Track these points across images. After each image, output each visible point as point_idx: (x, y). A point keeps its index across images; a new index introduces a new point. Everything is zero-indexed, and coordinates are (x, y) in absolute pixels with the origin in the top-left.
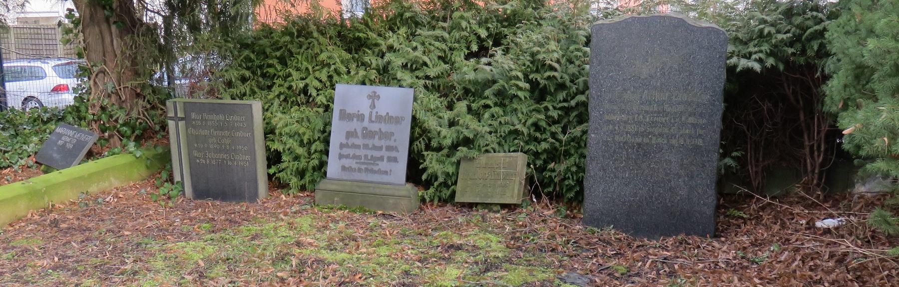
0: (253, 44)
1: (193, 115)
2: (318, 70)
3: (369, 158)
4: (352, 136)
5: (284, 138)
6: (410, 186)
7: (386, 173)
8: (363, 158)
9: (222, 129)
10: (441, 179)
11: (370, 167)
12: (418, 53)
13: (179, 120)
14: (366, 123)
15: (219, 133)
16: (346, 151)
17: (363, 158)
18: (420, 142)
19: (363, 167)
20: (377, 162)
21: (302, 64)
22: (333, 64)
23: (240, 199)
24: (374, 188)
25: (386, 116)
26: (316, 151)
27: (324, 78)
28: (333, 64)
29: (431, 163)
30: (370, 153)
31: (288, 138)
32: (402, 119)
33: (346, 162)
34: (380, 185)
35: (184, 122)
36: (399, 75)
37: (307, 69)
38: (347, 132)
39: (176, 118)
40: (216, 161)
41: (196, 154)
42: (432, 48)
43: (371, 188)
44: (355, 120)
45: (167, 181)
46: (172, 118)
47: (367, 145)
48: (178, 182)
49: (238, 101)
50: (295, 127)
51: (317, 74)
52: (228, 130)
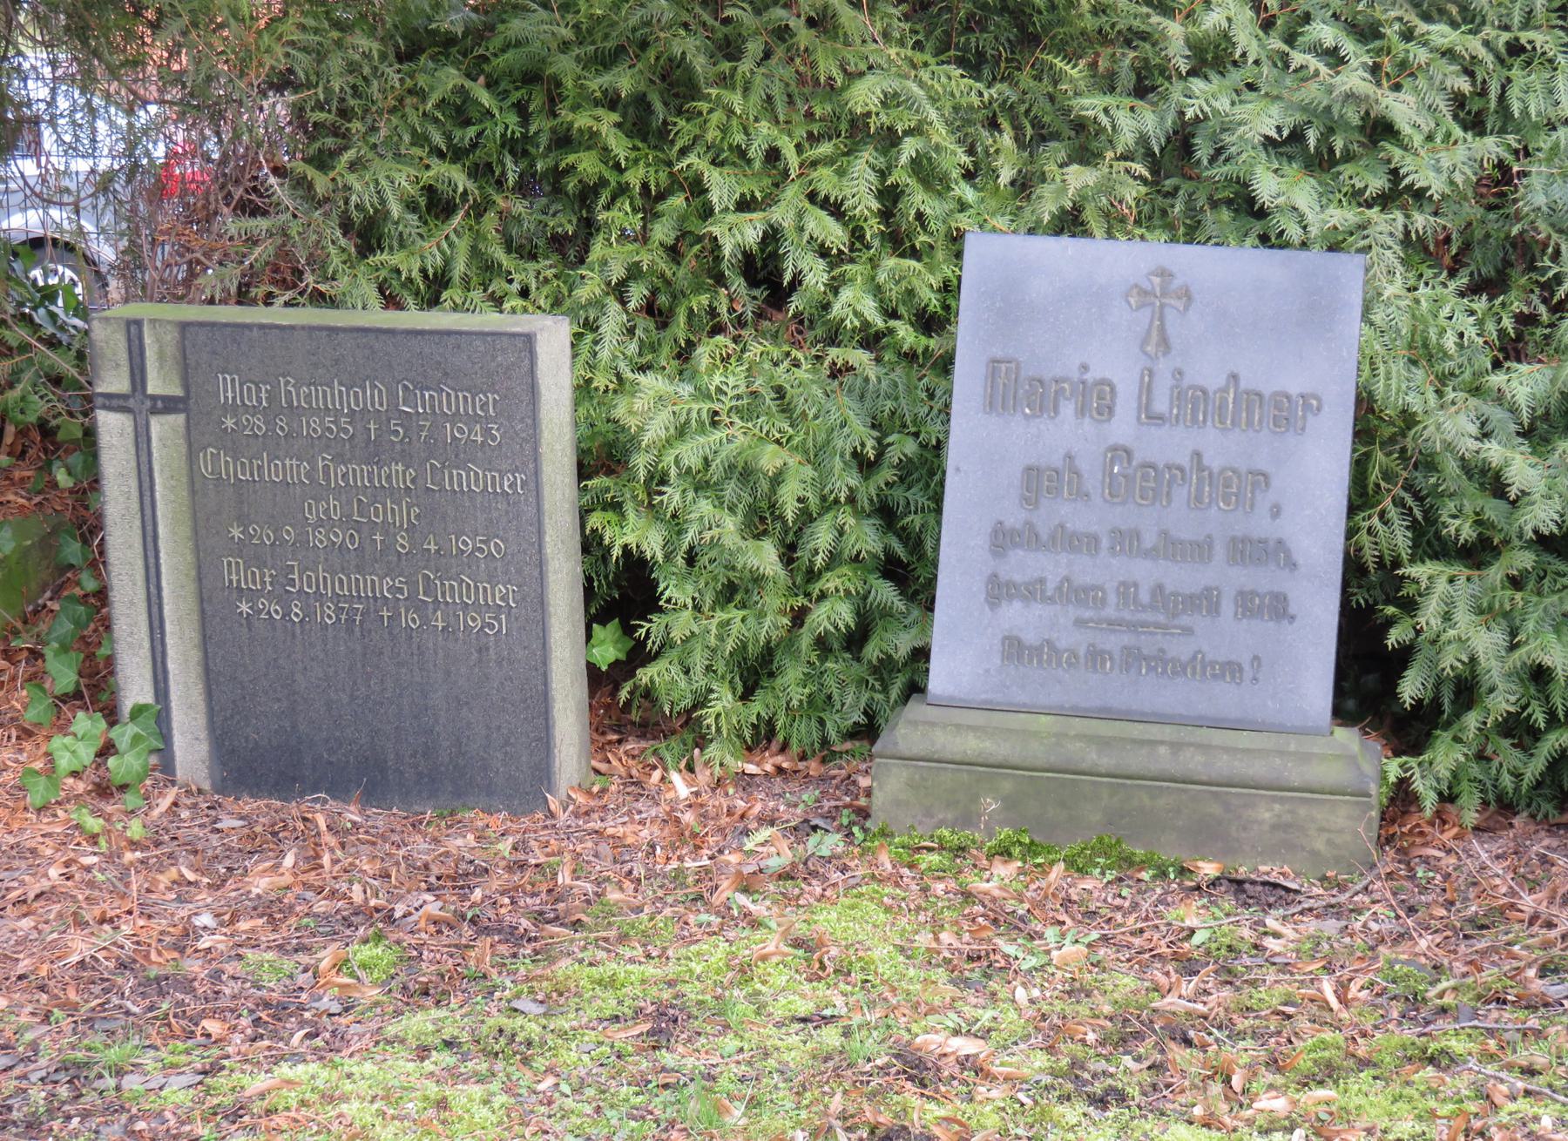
0: (479, 34)
1: (228, 388)
2: (828, 161)
3: (1145, 597)
4: (1055, 491)
5: (672, 496)
6: (1347, 737)
7: (1231, 670)
8: (1112, 598)
9: (374, 453)
10: (1501, 701)
11: (1148, 645)
12: (1354, 79)
13: (154, 411)
14: (1123, 427)
15: (359, 472)
16: (1022, 565)
17: (1112, 598)
18: (1382, 515)
19: (1114, 642)
20: (1185, 620)
21: (747, 133)
22: (909, 132)
23: (458, 794)
24: (1176, 746)
25: (1225, 390)
26: (834, 559)
27: (864, 202)
28: (909, 132)
29: (1447, 617)
30: (1145, 573)
31: (691, 495)
32: (1310, 403)
33: (1018, 617)
34: (1204, 735)
35: (179, 419)
36: (1267, 186)
37: (773, 155)
38: (1029, 469)
39: (138, 404)
40: (339, 610)
41: (234, 573)
42: (1421, 55)
43: (1162, 750)
44: (1068, 409)
45: (74, 698)
46: (116, 403)
47: (1136, 535)
48: (138, 711)
49: (413, 318)
50: (732, 440)
51: (825, 179)
52: (406, 458)
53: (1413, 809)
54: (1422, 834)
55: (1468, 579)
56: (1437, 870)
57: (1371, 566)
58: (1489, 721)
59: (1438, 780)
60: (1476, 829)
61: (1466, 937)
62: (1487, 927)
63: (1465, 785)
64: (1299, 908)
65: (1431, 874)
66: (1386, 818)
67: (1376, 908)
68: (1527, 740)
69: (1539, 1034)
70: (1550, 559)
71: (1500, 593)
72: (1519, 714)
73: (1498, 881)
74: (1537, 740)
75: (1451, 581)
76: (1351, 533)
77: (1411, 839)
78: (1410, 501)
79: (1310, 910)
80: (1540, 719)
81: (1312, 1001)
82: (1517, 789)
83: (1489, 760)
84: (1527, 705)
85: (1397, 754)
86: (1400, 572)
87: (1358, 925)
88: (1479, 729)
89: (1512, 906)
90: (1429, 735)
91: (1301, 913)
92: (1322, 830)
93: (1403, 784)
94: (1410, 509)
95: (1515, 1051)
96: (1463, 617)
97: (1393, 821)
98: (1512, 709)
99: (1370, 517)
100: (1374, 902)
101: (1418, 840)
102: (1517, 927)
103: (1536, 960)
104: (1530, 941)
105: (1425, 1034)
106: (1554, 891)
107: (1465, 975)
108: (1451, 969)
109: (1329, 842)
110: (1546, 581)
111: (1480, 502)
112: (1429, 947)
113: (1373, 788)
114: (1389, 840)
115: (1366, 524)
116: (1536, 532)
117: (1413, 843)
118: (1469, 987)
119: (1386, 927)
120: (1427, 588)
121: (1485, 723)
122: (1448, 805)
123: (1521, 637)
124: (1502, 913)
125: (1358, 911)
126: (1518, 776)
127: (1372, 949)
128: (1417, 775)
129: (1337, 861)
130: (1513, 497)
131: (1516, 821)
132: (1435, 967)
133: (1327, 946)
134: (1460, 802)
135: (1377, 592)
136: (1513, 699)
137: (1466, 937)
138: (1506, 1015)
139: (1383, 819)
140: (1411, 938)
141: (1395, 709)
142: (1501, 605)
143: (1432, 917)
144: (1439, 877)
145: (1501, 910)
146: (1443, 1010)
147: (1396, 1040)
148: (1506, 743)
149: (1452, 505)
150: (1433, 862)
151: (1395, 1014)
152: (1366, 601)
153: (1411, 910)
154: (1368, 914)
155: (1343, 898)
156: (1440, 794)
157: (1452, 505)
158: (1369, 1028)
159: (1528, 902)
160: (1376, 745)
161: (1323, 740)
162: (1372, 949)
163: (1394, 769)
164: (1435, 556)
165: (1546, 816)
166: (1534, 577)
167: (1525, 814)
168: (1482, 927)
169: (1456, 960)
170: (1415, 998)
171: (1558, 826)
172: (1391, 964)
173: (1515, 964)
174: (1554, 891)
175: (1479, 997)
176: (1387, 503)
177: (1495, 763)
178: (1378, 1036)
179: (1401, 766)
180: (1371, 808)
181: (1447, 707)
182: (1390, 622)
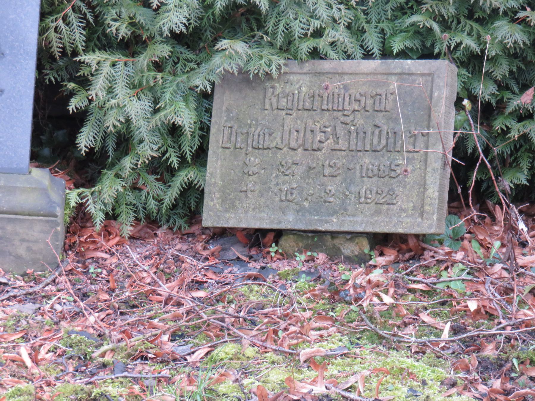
29: (110, 91)
53: (88, 224)
54: (94, 242)
55: (125, 64)
56: (103, 267)
57: (57, 55)
58: (140, 163)
59: (105, 204)
60: (131, 238)
61: (122, 314)
62: (137, 307)
63: (123, 207)
64: (7, 296)
65: (99, 270)
66: (69, 231)
67: (60, 294)
68: (166, 176)
69: (169, 381)
70: (182, 50)
71: (146, 74)
72: (160, 158)
73: (145, 274)
74: (173, 175)
75: (114, 65)
76: (42, 31)
77: (86, 246)
78: (84, 9)
79: (15, 297)
80: (174, 161)
81: (13, 361)
82: (159, 210)
83: (140, 190)
84: (167, 151)
85: (77, 186)
86: (77, 59)
87: (47, 307)
88: (133, 169)
89: (154, 292)
90: (100, 173)
91: (8, 299)
92: (23, 240)
93: (81, 207)
94: (85, 14)
95: (152, 393)
96: (121, 90)
97: (75, 233)
98: (155, 155)
99: (56, 20)
100: (59, 291)
101: (92, 247)
102: (157, 306)
103: (168, 329)
104: (165, 316)
105: (90, 383)
106: (183, 280)
107: (119, 341)
108: (110, 337)
109: (29, 249)
110: (179, 65)
111: (133, 10)
112: (96, 322)
113: (59, 211)
114: (71, 247)
115: (54, 25)
116: (171, 31)
117: (88, 249)
118: (122, 349)
119: (66, 308)
120: (97, 70)
121: (136, 165)
122: (113, 222)
123: (161, 104)
124: (147, 297)
125: (48, 297)
126: (160, 201)
127: (56, 323)
128: (91, 201)
129: (34, 262)
130: (155, 6)
131: (159, 232)
132: (99, 336)
133: (24, 323)
134: (120, 219)
135: (64, 73)
136: (156, 147)
137: (122, 314)
138: (147, 368)
139: (68, 232)
140: (84, 315)
141: (76, 154)
142: (148, 82)
143: (99, 300)
144: (105, 272)
145: (147, 295)
146: (104, 366)
147: (70, 387)
148: (152, 178)
149: (114, 12)
150: (101, 262)
151: (71, 369)
152: (56, 79)
153: (85, 296)
154: (54, 299)
155: (37, 288)
156: (107, 214)
157: (114, 12)
158: (52, 379)
159: (165, 289)
160: (61, 180)
161: (24, 177)
162: (56, 323)
163: (74, 197)
164: (103, 48)
165: (180, 229)
166: (171, 62)
167: (165, 227)
168: (133, 307)
169: (114, 330)
170: (85, 358)
171: (188, 235)
172: (69, 334)
173: (154, 332)
174: (183, 280)
175: (129, 356)
176: (69, 10)
177: (144, 193)
178: (59, 384)
179: (79, 195)
180: (58, 225)
181: (111, 153)
182: (72, 94)
